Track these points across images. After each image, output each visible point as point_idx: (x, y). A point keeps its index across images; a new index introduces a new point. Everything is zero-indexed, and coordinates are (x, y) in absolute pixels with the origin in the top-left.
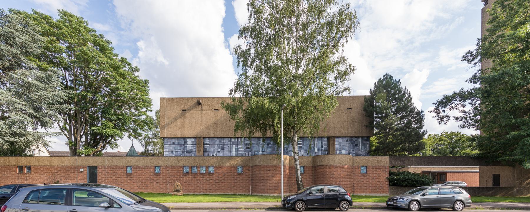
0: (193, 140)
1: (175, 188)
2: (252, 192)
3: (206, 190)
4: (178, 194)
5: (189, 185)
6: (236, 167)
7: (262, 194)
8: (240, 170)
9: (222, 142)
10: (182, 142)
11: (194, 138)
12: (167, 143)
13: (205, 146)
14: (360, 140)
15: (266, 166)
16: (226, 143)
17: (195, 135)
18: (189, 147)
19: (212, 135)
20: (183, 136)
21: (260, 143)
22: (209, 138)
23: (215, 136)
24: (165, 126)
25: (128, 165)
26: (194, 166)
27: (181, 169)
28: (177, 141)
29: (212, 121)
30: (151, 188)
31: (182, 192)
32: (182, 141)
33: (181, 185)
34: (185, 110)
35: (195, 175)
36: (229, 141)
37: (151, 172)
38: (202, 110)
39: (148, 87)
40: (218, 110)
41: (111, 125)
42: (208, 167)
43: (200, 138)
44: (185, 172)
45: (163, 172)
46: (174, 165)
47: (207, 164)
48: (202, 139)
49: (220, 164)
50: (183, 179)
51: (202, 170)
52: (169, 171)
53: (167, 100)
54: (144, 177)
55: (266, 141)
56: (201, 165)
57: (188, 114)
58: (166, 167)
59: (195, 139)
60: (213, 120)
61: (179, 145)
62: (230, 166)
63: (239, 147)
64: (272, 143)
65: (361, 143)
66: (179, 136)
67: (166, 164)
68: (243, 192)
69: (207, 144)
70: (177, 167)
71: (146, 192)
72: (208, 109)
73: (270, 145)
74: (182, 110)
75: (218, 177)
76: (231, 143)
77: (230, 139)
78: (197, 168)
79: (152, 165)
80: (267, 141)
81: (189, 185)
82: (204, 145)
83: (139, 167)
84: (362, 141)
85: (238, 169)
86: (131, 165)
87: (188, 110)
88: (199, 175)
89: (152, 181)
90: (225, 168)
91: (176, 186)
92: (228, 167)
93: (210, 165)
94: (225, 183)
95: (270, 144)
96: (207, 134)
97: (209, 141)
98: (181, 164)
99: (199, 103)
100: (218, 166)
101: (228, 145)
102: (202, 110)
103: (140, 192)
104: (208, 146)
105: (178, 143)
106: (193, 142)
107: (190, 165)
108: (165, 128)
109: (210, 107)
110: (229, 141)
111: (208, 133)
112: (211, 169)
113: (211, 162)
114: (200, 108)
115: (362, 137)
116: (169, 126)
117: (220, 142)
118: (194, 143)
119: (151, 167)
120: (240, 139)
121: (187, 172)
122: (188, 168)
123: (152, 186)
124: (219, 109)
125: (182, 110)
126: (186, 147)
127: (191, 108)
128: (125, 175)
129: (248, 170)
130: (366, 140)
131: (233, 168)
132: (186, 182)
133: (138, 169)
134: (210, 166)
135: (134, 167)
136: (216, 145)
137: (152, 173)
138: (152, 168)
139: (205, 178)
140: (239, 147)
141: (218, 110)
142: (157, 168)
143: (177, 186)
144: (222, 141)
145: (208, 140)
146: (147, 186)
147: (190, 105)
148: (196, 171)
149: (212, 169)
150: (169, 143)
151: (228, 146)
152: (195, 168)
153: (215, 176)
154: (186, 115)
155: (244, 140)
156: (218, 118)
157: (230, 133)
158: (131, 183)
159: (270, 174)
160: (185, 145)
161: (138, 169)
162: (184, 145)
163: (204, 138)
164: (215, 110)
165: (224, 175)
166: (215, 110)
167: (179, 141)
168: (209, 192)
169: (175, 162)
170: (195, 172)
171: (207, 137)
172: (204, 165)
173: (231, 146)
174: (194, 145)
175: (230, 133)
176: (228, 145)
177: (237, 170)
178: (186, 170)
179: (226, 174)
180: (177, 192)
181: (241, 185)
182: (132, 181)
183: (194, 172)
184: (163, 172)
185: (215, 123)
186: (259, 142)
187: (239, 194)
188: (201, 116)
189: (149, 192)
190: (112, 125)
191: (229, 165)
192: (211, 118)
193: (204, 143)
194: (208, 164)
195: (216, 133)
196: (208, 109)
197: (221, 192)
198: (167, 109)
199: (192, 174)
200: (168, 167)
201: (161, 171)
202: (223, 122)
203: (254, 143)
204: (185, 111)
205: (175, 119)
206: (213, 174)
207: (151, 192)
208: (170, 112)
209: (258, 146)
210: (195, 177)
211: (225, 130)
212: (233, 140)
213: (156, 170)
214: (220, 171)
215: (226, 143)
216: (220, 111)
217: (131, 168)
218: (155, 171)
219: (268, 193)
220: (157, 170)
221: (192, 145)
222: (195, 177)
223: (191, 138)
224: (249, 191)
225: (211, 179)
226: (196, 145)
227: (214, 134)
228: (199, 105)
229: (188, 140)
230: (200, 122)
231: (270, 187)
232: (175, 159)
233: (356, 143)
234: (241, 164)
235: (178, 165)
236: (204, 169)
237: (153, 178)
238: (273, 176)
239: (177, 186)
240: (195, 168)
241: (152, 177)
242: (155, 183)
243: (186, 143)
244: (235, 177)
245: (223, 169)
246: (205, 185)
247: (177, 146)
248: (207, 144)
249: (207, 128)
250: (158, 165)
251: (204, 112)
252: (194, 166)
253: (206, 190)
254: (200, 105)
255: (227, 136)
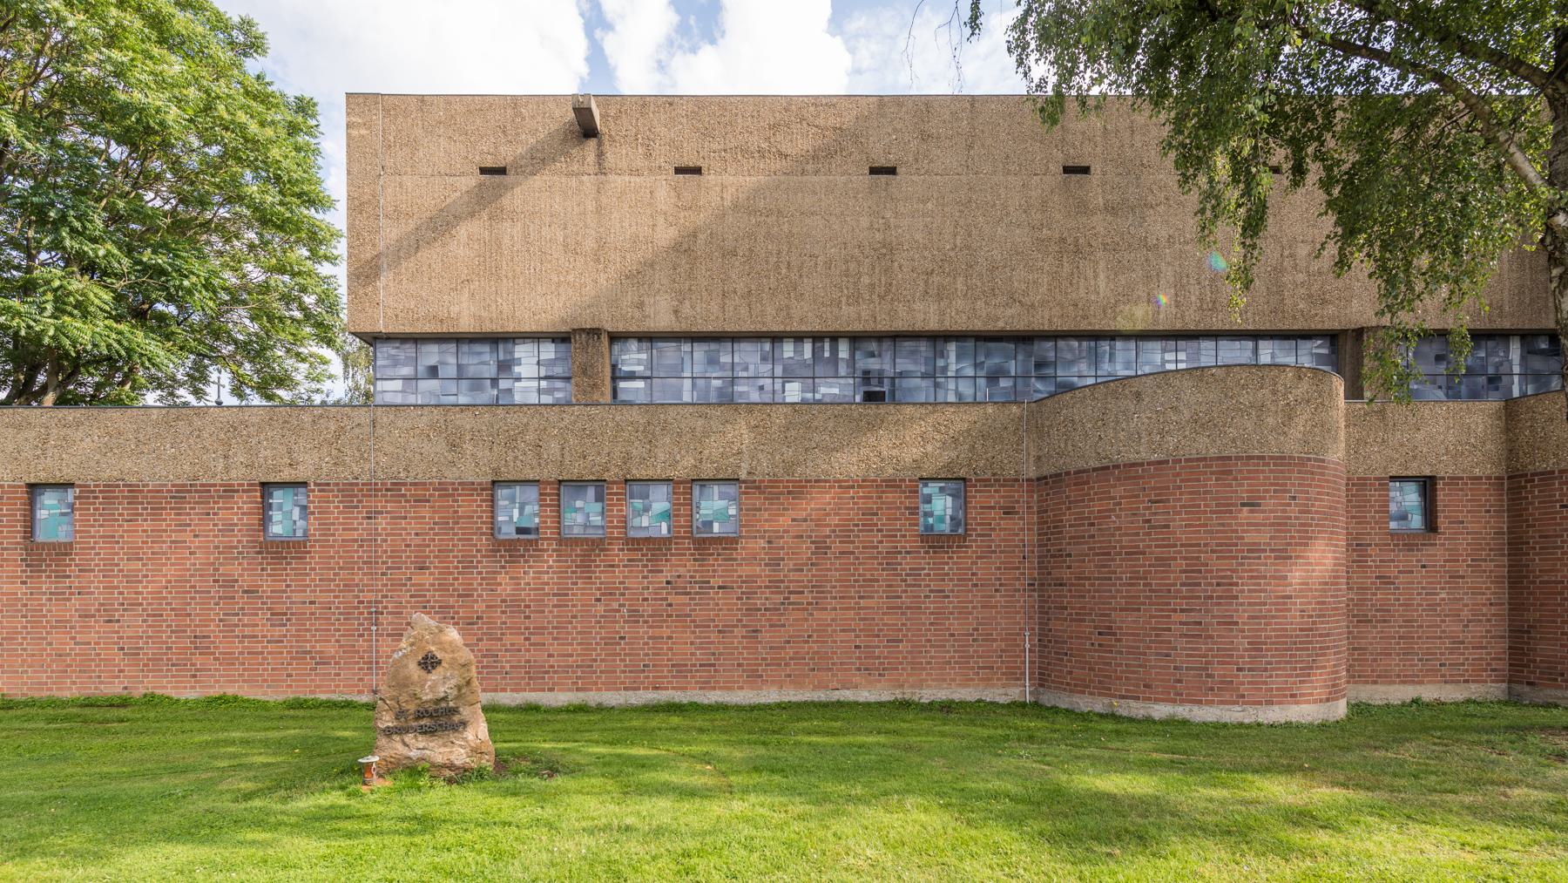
0: (549, 351)
1: (402, 684)
2: (1043, 680)
3: (680, 669)
4: (438, 751)
5: (540, 630)
6: (909, 486)
7: (1182, 711)
8: (942, 505)
9: (722, 367)
10: (483, 361)
11: (561, 338)
12: (390, 372)
13: (622, 385)
14: (1515, 351)
15: (1224, 465)
16: (746, 369)
17: (564, 321)
18: (526, 390)
19: (662, 320)
20: (489, 327)
21: (945, 369)
22: (649, 338)
23: (683, 326)
24: (378, 267)
25: (42, 477)
26: (579, 484)
27: (472, 507)
28: (452, 360)
29: (666, 235)
30: (229, 660)
31: (478, 731)
32: (487, 357)
33: (466, 655)
34: (502, 171)
35: (591, 548)
36: (764, 359)
37: (229, 528)
38: (601, 170)
39: (316, 152)
40: (697, 171)
41: (100, 297)
42: (687, 488)
43: (595, 332)
44: (508, 532)
45: (325, 528)
46: (419, 472)
47: (684, 467)
48: (605, 339)
49: (789, 467)
50: (491, 581)
51: (647, 509)
52: (382, 523)
53: (386, 111)
54: (170, 571)
55: (981, 359)
56: (637, 473)
57: (521, 194)
58: (350, 492)
59: (563, 347)
60: (672, 233)
61: (464, 384)
62: (864, 483)
63: (823, 390)
64: (1012, 367)
65: (1516, 369)
66: (466, 325)
67: (356, 469)
68: (966, 682)
69: (632, 376)
70: (442, 487)
71: (191, 695)
72: (640, 163)
73: (1004, 383)
74: (484, 171)
75: (775, 563)
76: (779, 371)
77: (767, 346)
78: (599, 498)
79: (237, 475)
80: (987, 355)
81: (540, 630)
82: (614, 379)
83: (134, 493)
84: (1523, 358)
85: (928, 500)
86: (68, 474)
87: (520, 169)
88: (618, 554)
89: (241, 600)
90: (824, 499)
91: (414, 670)
92: (844, 485)
93: (708, 471)
94: (827, 616)
95: (1006, 375)
96: (637, 314)
97: (644, 356)
98: (473, 466)
99: (585, 128)
100: (775, 482)
101: (761, 382)
102: (601, 170)
103: (138, 692)
104: (640, 384)
105: (459, 366)
106: (551, 363)
107: (550, 473)
108: (377, 276)
109: (648, 155)
110: (764, 359)
111: (640, 306)
112: (715, 507)
113: (713, 447)
114: (591, 158)
115: (1527, 337)
116: (404, 264)
117: (712, 361)
118: (558, 370)
119: (229, 491)
120: (827, 345)
121: (520, 531)
122: (532, 493)
123: (237, 647)
124: (704, 165)
125: (484, 171)
126: (509, 391)
127: (538, 160)
128: (18, 555)
129: (1009, 511)
130: (1542, 352)
131: (889, 497)
132: (514, 605)
133: (121, 509)
134: (703, 482)
135: (86, 494)
136: (687, 384)
137: (240, 538)
138: (245, 504)
139: (667, 574)
140: (823, 390)
141: (697, 171)
142: (278, 497)
143: (429, 663)
144: (725, 359)
145: (639, 351)
146: (201, 643)
147: (533, 141)
148: (596, 520)
149: (720, 504)
150: (407, 371)
151: (761, 388)
152: (591, 492)
153: (752, 559)
154: (506, 201)
155: (852, 355)
156: (701, 219)
157: (770, 310)
158: (62, 623)
159: (1263, 537)
160: (503, 384)
161: (121, 509)
162: (495, 381)
163: (615, 338)
164: (679, 171)
165: (821, 547)
166: (679, 171)
167: (465, 360)
168: (706, 686)
169: (427, 447)
170: (586, 526)
171: (633, 328)
172: (658, 472)
173: (778, 386)
174: (559, 384)
175: (770, 310)
176: (761, 382)
177: (914, 510)
178: (515, 511)
179: (837, 546)
180: (428, 732)
181: (954, 624)
182: (75, 602)
183: (577, 532)
184: (325, 528)
185: (684, 248)
186: (940, 363)
187: (942, 694)
188: (599, 210)
189: (215, 692)
190: (108, 296)
191: (855, 471)
192: (661, 220)
193: (614, 367)
194: (690, 461)
195: (686, 309)
196: (640, 163)
197: (798, 683)
198: (389, 162)
199: (566, 542)
200: (372, 489)
201: (314, 523)
202: (729, 244)
203: (911, 367)
204: (497, 178)
205: (440, 225)
206: (727, 542)
207: (231, 691)
208: (408, 181)
209: (936, 385)
210: (586, 565)
211: (740, 287)
212: (788, 350)
213: (276, 516)
214: (784, 521)
215: (746, 369)
216: (709, 178)
217: (71, 495)
218: (265, 521)
219: (1240, 699)
220: (285, 519)
221: (544, 384)
222: (586, 565)
223: (536, 337)
224: (1014, 676)
225: (716, 582)
226: (567, 379)
227: (676, 312)
228: (581, 143)
229: (523, 351)
230: (590, 244)
231: (1256, 647)
232: (423, 422)
233: (1491, 370)
234: (949, 466)
235: (451, 475)
236: (660, 500)
237: (246, 581)
238: (1283, 556)
239: (429, 663)
240: (591, 492)
241: (235, 570)
242: (262, 617)
243: (505, 367)
244: (907, 563)
245: (810, 505)
246: (666, 632)
247: (452, 387)
248: (632, 376)
249: (637, 277)
250: (286, 475)
251: (617, 181)
252: (579, 484)
253: (680, 669)
254: (592, 143)
255: (748, 326)
